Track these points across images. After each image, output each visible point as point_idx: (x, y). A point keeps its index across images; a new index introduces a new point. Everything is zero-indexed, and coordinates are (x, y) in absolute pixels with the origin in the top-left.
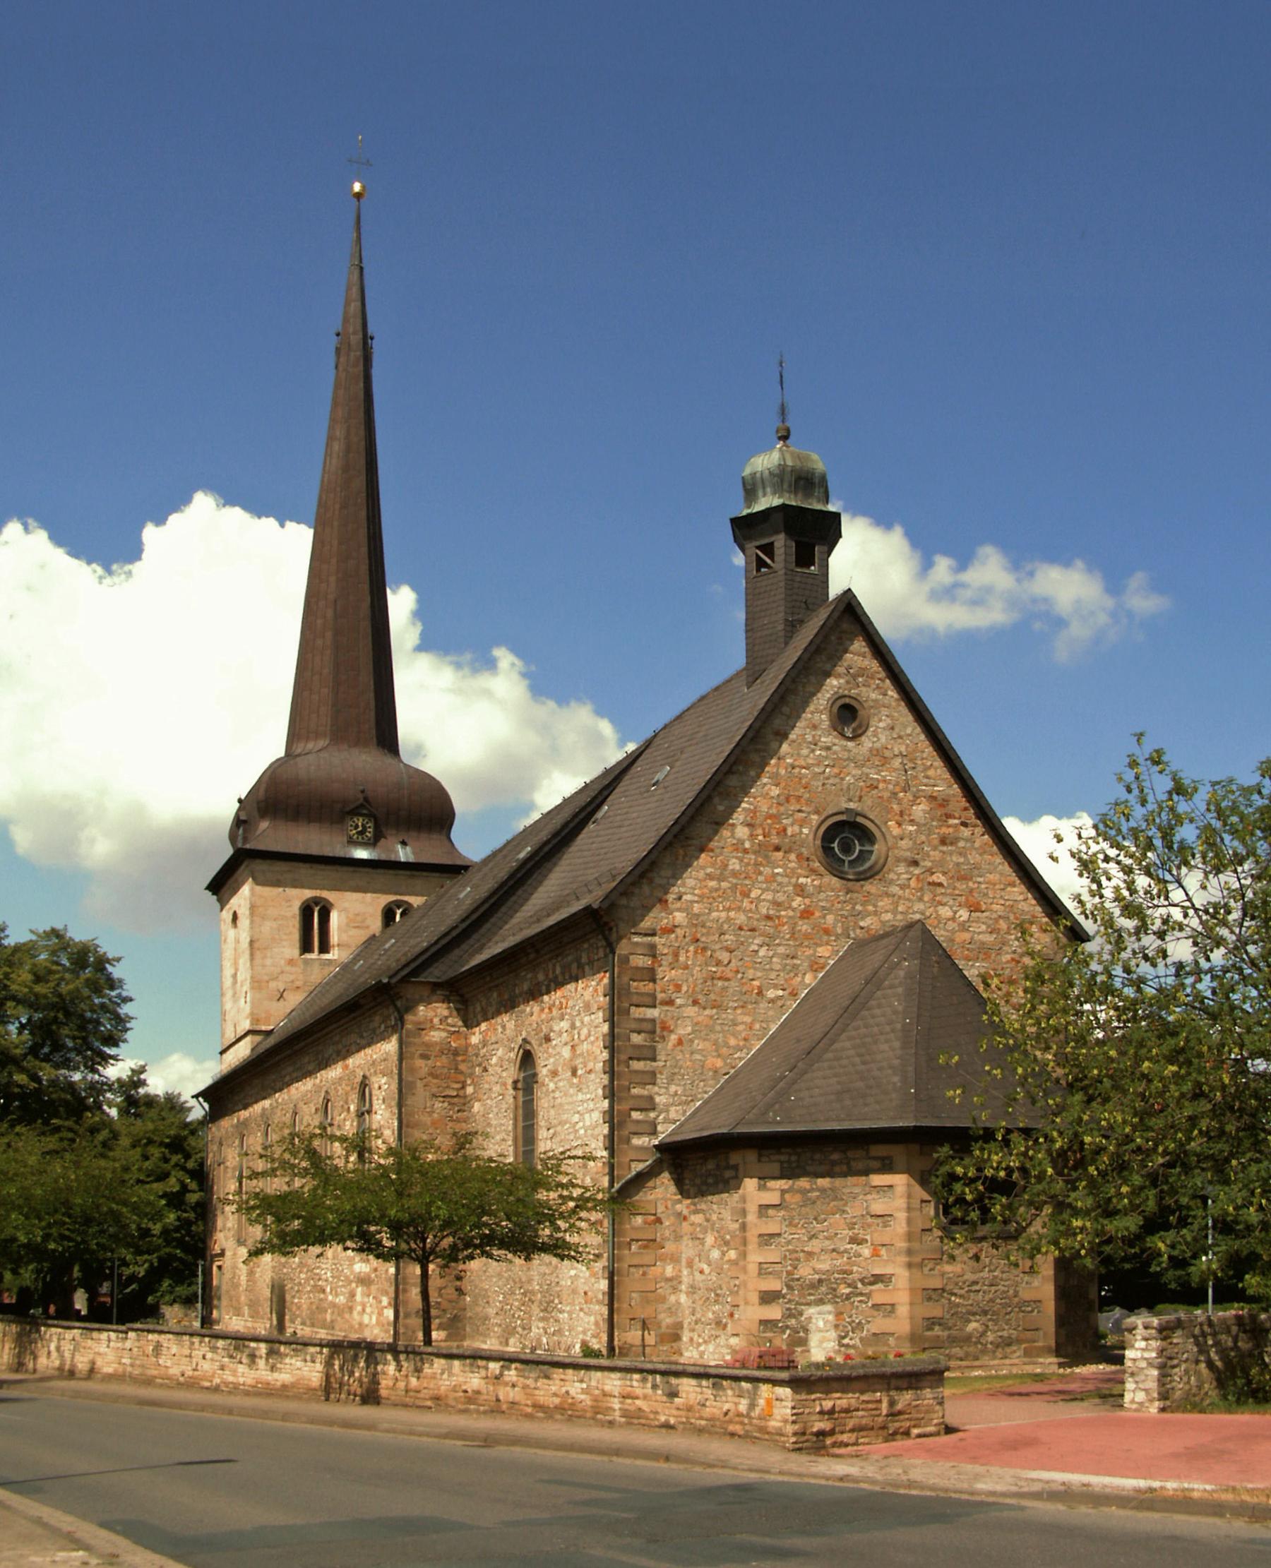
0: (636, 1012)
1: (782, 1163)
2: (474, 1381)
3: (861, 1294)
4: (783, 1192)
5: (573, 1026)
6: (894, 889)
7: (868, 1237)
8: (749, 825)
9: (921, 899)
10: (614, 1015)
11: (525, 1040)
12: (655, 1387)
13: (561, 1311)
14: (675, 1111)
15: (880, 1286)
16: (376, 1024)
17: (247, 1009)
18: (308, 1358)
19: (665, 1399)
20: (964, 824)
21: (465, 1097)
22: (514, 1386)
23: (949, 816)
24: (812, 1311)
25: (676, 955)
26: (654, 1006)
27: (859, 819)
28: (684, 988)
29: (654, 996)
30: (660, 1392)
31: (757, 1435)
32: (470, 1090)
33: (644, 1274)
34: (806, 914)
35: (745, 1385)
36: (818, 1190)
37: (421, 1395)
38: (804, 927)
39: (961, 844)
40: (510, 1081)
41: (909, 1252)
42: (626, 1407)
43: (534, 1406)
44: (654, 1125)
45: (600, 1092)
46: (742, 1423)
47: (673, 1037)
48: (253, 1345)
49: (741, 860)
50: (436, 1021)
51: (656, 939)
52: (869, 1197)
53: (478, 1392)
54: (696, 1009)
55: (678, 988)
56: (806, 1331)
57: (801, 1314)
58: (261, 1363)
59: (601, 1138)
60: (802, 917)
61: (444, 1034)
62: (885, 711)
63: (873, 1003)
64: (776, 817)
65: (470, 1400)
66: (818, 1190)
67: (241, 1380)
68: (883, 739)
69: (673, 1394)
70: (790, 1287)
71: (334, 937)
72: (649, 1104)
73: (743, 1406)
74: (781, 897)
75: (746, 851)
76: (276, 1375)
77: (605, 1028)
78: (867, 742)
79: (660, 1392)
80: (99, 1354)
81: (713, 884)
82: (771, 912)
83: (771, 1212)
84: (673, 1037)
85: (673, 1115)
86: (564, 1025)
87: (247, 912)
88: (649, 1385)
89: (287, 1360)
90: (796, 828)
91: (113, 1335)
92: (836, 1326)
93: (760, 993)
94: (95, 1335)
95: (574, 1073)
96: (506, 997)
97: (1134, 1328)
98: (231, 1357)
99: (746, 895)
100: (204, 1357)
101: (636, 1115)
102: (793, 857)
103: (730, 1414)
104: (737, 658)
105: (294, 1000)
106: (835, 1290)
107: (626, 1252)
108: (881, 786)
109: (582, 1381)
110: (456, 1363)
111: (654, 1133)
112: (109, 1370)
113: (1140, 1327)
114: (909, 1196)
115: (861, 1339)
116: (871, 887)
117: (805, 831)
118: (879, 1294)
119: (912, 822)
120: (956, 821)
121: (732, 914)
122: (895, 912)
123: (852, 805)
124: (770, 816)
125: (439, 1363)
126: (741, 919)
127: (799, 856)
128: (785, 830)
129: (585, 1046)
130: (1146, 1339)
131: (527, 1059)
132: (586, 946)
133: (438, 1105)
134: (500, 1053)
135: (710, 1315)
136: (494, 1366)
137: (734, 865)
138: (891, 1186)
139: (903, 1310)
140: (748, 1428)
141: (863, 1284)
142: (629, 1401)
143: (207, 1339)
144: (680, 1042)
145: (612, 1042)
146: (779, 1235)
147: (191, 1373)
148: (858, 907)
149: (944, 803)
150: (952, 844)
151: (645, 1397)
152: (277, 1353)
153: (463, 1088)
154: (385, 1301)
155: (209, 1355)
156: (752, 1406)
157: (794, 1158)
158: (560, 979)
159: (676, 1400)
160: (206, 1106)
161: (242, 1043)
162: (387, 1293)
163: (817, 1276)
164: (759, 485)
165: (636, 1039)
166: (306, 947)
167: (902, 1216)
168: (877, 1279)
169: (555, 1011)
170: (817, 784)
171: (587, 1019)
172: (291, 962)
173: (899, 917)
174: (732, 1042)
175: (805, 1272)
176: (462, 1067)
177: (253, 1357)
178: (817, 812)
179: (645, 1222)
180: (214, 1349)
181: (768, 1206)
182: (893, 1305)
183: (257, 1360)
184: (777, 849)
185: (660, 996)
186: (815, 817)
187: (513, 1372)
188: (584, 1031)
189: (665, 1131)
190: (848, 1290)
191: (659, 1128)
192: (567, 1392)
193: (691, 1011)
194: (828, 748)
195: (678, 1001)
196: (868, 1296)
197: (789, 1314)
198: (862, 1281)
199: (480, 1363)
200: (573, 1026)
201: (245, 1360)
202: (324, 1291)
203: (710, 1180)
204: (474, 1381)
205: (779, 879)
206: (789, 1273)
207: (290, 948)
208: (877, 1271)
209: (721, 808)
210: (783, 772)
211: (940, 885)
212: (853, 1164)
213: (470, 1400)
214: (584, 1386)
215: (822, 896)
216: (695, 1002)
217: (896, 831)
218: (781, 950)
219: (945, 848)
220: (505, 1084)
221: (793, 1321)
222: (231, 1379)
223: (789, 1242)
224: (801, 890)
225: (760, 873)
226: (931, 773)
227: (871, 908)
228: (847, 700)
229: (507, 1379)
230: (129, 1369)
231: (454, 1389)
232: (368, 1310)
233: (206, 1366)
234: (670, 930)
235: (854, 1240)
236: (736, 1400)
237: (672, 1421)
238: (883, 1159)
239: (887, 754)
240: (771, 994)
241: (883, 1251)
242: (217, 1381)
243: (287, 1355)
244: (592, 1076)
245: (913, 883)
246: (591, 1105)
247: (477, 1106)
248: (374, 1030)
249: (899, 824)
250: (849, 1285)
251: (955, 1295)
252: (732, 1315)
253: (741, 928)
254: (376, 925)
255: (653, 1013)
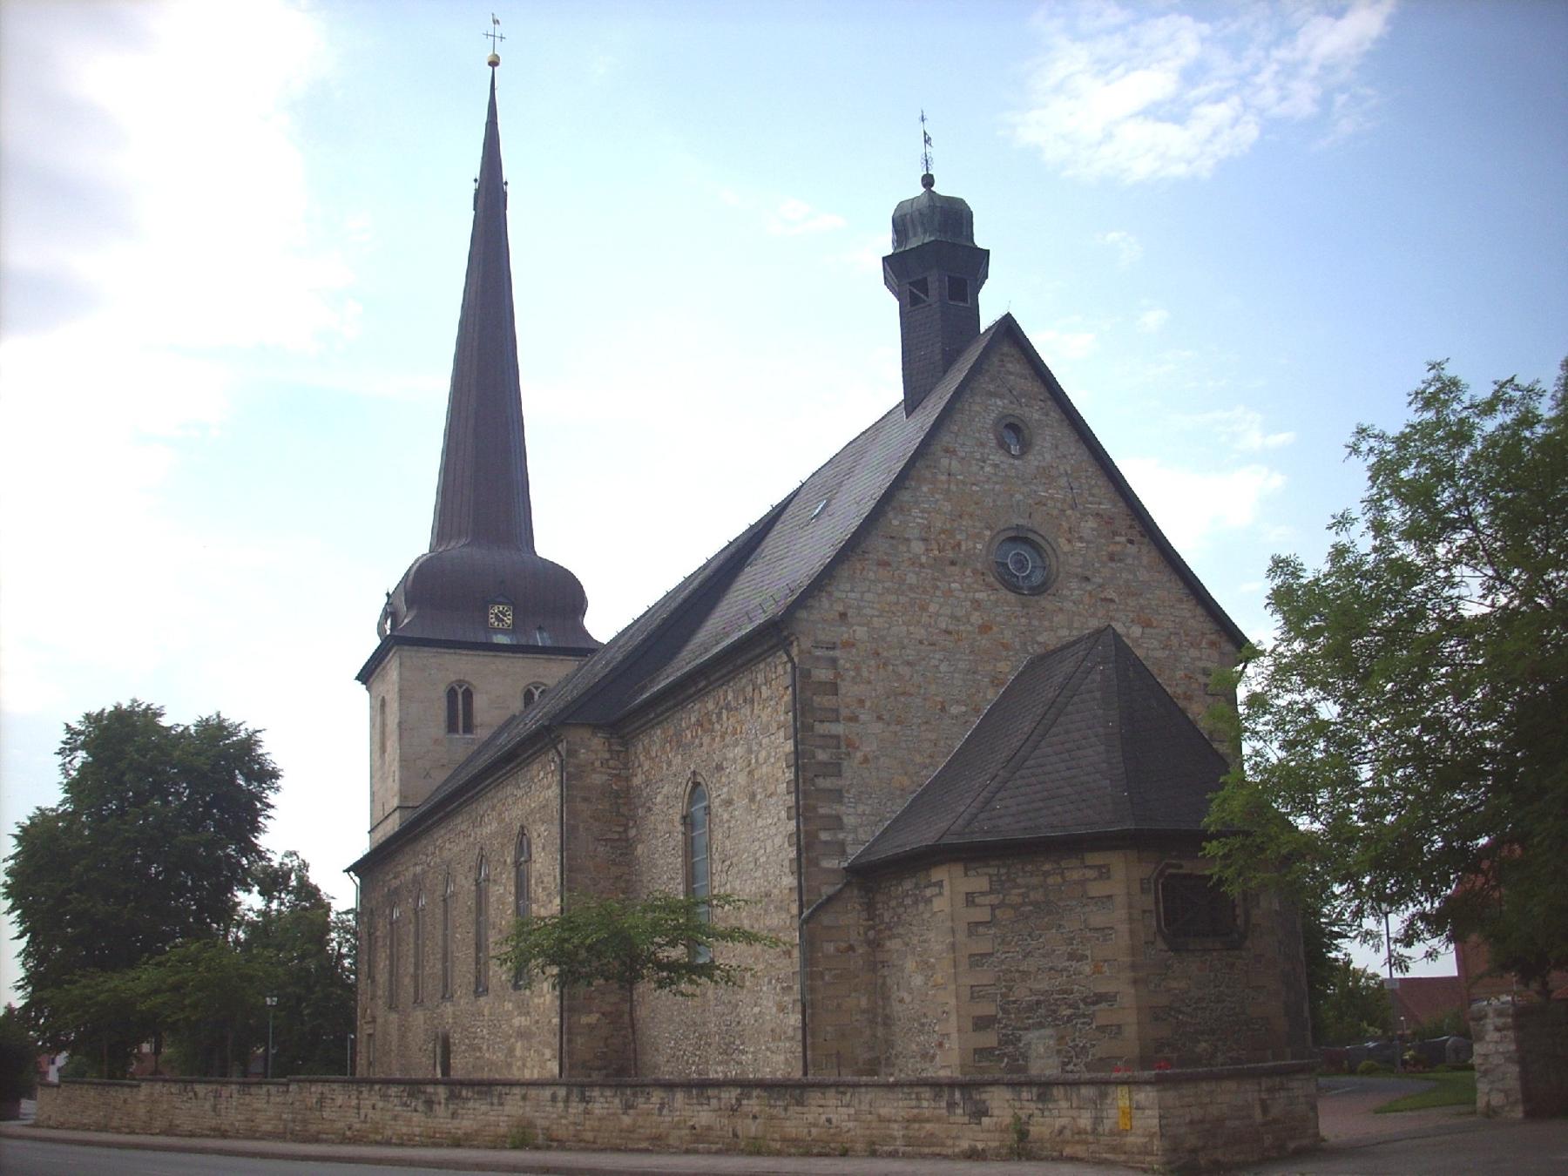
0: (821, 728)
1: (990, 876)
2: (704, 1116)
3: (1084, 1016)
4: (993, 908)
5: (750, 751)
6: (1068, 605)
7: (1088, 953)
8: (925, 540)
9: (1093, 615)
10: (801, 731)
11: (694, 773)
12: (951, 1105)
13: (743, 1052)
14: (860, 828)
15: (1103, 1005)
16: (534, 773)
17: (396, 787)
18: (495, 1101)
19: (966, 1119)
20: (1131, 542)
21: (627, 840)
22: (755, 1117)
23: (1115, 534)
24: (1031, 1036)
25: (858, 669)
26: (837, 721)
27: (1030, 535)
28: (868, 704)
29: (837, 711)
30: (959, 1111)
31: (1110, 1156)
32: (632, 833)
33: (839, 1006)
34: (985, 629)
35: (1087, 1092)
36: (1031, 904)
37: (635, 1136)
38: (984, 642)
39: (1129, 561)
40: (678, 818)
41: (1133, 967)
42: (911, 1133)
43: (784, 1140)
44: (842, 844)
45: (783, 814)
46: (1086, 1142)
47: (859, 755)
48: (430, 1089)
49: (918, 574)
50: (597, 764)
51: (837, 653)
52: (1087, 909)
53: (709, 1128)
54: (881, 725)
55: (861, 702)
56: (1026, 1058)
57: (1019, 1040)
58: (440, 1110)
59: (786, 863)
60: (980, 633)
61: (605, 777)
62: (1048, 431)
63: (1070, 708)
64: (950, 533)
65: (698, 1138)
66: (1031, 904)
67: (417, 1130)
68: (1048, 457)
69: (980, 1112)
70: (1005, 1011)
71: (478, 718)
72: (837, 823)
73: (1085, 1121)
74: (960, 613)
75: (922, 566)
76: (456, 1122)
77: (789, 746)
78: (1033, 460)
79: (959, 1111)
80: (257, 1110)
81: (893, 598)
82: (951, 628)
83: (981, 930)
84: (859, 755)
85: (863, 837)
86: (739, 751)
87: (396, 696)
88: (944, 1104)
89: (471, 1104)
90: (970, 544)
91: (273, 1089)
92: (1059, 1052)
93: (943, 709)
94: (253, 1090)
95: (752, 797)
96: (671, 732)
97: (1486, 1016)
98: (405, 1105)
99: (923, 608)
100: (374, 1107)
101: (824, 836)
102: (968, 572)
103: (1068, 1133)
104: (895, 394)
105: (440, 777)
106: (1055, 1012)
107: (820, 983)
108: (1050, 503)
109: (848, 1106)
110: (680, 1096)
111: (843, 853)
112: (269, 1127)
113: (1491, 1015)
114: (1130, 906)
115: (1086, 1065)
116: (1046, 602)
117: (979, 546)
118: (1103, 1014)
119: (1081, 539)
120: (1123, 539)
121: (912, 629)
122: (1070, 628)
123: (1021, 522)
124: (943, 531)
125: (657, 1096)
126: (920, 633)
127: (975, 571)
128: (959, 545)
129: (764, 769)
130: (1498, 1029)
131: (696, 790)
132: (762, 666)
133: (600, 849)
134: (665, 791)
135: (914, 1046)
136: (729, 1096)
137: (912, 579)
138: (1110, 897)
139: (1131, 1031)
140: (1092, 1147)
141: (1086, 1004)
142: (916, 1126)
143: (377, 1087)
144: (866, 760)
145: (799, 761)
146: (992, 954)
147: (357, 1126)
148: (1035, 623)
149: (1110, 521)
150: (1120, 560)
151: (939, 1120)
152: (459, 1097)
153: (626, 831)
154: (548, 1053)
155: (380, 1104)
156: (1098, 1120)
157: (1003, 871)
158: (733, 704)
159: (985, 1120)
160: (357, 880)
161: (390, 820)
162: (549, 1045)
163: (1034, 998)
164: (909, 225)
165: (822, 756)
166: (452, 727)
167: (1123, 928)
168: (1100, 998)
169: (728, 739)
170: (989, 502)
171: (765, 741)
172: (436, 741)
173: (1075, 633)
174: (918, 759)
175: (1021, 992)
176: (624, 810)
177: (429, 1103)
178: (989, 528)
179: (837, 950)
180: (385, 1097)
181: (978, 924)
182: (1119, 1026)
183: (436, 1107)
184: (953, 563)
185: (844, 712)
186: (988, 533)
187: (753, 1102)
188: (763, 754)
189: (854, 851)
190: (1069, 1012)
191: (849, 850)
192: (829, 1121)
193: (878, 727)
194: (996, 466)
195: (863, 717)
196: (1092, 1017)
197: (1005, 1041)
198: (1084, 1000)
199: (710, 1092)
200: (750, 751)
201: (421, 1108)
202: (480, 1049)
203: (908, 901)
204: (704, 1116)
205: (956, 593)
206: (1004, 996)
207: (438, 728)
208: (1102, 990)
209: (896, 522)
210: (953, 487)
211: (1112, 601)
212: (1067, 874)
213: (698, 1138)
214: (852, 1111)
215: (998, 610)
216: (880, 718)
217: (1067, 548)
218: (962, 665)
219: (1113, 565)
220: (672, 821)
221: (1011, 1048)
222: (404, 1130)
223: (1002, 962)
224: (977, 605)
225: (937, 587)
226: (1095, 491)
227: (1046, 623)
228: (1012, 420)
229: (745, 1109)
230: (291, 1125)
231: (676, 1126)
232: (529, 1064)
233: (374, 1116)
234: (849, 645)
235: (1072, 956)
236: (1075, 1113)
237: (980, 1146)
238: (1100, 867)
239: (1054, 472)
240: (954, 710)
241: (1105, 968)
242: (389, 1133)
243: (468, 1099)
244: (773, 800)
245: (1086, 599)
246: (773, 830)
247: (640, 849)
248: (532, 779)
249: (1069, 541)
250: (1070, 1006)
251: (1181, 1012)
252: (941, 1045)
253: (921, 642)
254: (517, 705)
255: (838, 729)
